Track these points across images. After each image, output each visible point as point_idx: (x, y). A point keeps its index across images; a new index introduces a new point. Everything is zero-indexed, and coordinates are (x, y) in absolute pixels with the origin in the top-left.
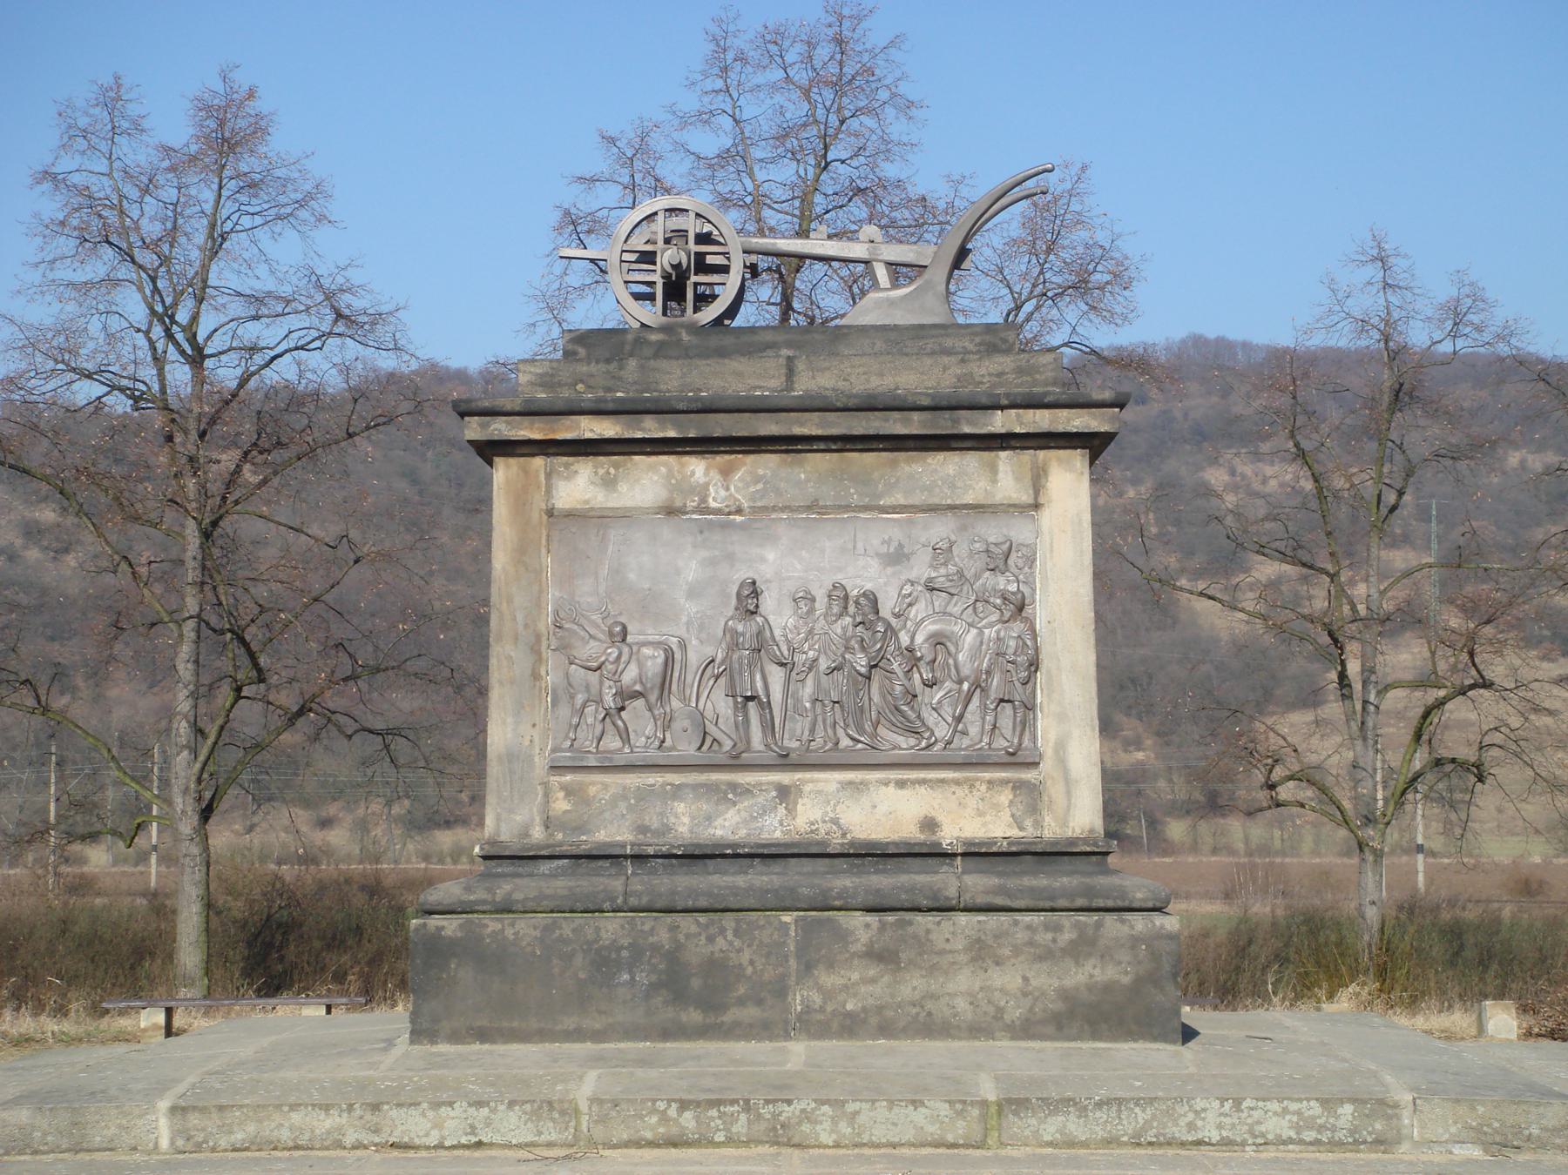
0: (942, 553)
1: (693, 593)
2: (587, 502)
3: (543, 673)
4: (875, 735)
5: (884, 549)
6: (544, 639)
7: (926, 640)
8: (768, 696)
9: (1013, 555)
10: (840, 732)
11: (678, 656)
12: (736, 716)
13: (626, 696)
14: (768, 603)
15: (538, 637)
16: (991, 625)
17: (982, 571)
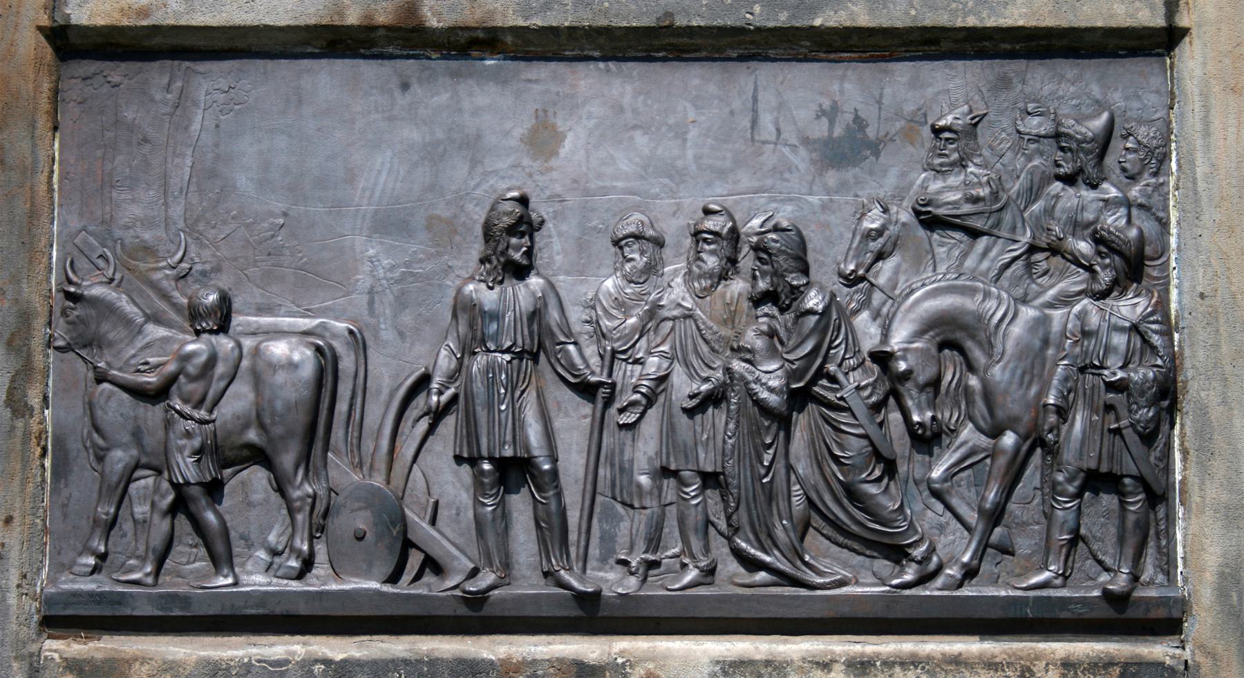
0: (954, 143)
1: (390, 223)
2: (144, 12)
3: (35, 401)
4: (797, 554)
5: (820, 130)
6: (39, 323)
7: (918, 334)
8: (554, 460)
9: (1117, 145)
10: (720, 549)
11: (347, 363)
12: (477, 503)
13: (227, 455)
14: (554, 246)
15: (25, 317)
16: (1065, 300)
17: (1046, 180)
